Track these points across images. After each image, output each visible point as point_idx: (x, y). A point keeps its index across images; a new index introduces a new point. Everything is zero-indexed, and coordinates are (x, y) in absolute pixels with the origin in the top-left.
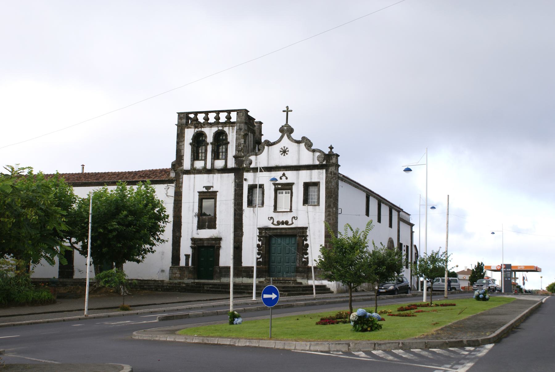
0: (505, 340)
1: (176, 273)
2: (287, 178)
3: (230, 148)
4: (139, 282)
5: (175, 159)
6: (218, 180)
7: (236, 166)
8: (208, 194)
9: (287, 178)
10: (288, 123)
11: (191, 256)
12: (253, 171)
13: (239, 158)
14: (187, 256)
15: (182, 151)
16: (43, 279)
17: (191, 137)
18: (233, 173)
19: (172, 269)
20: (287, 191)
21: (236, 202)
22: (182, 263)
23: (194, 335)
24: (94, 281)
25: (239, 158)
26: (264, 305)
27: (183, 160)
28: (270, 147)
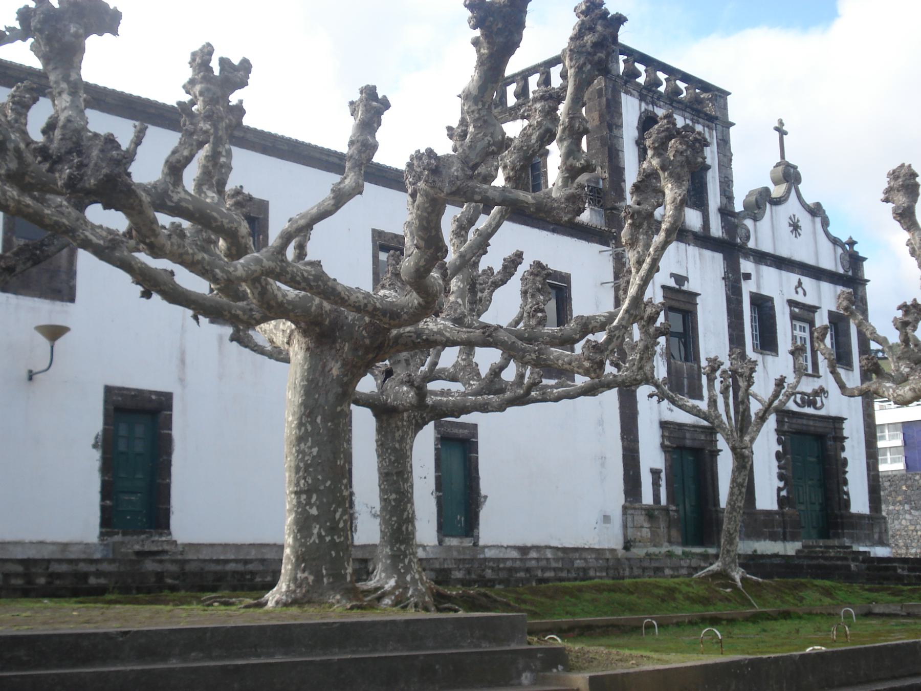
0: (499, 544)
1: (642, 527)
2: (805, 294)
3: (711, 184)
4: (560, 554)
5: (94, 35)
6: (695, 264)
7: (724, 235)
8: (681, 297)
9: (805, 294)
10: (787, 159)
11: (663, 475)
12: (754, 259)
13: (730, 216)
14: (655, 473)
15: (620, 153)
16: (238, 547)
17: (636, 123)
18: (378, 165)
19: (632, 514)
20: (803, 324)
21: (734, 333)
22: (647, 498)
23: (79, 616)
24: (431, 556)
25: (729, 217)
26: (753, 606)
27: (624, 181)
28: (774, 207)
